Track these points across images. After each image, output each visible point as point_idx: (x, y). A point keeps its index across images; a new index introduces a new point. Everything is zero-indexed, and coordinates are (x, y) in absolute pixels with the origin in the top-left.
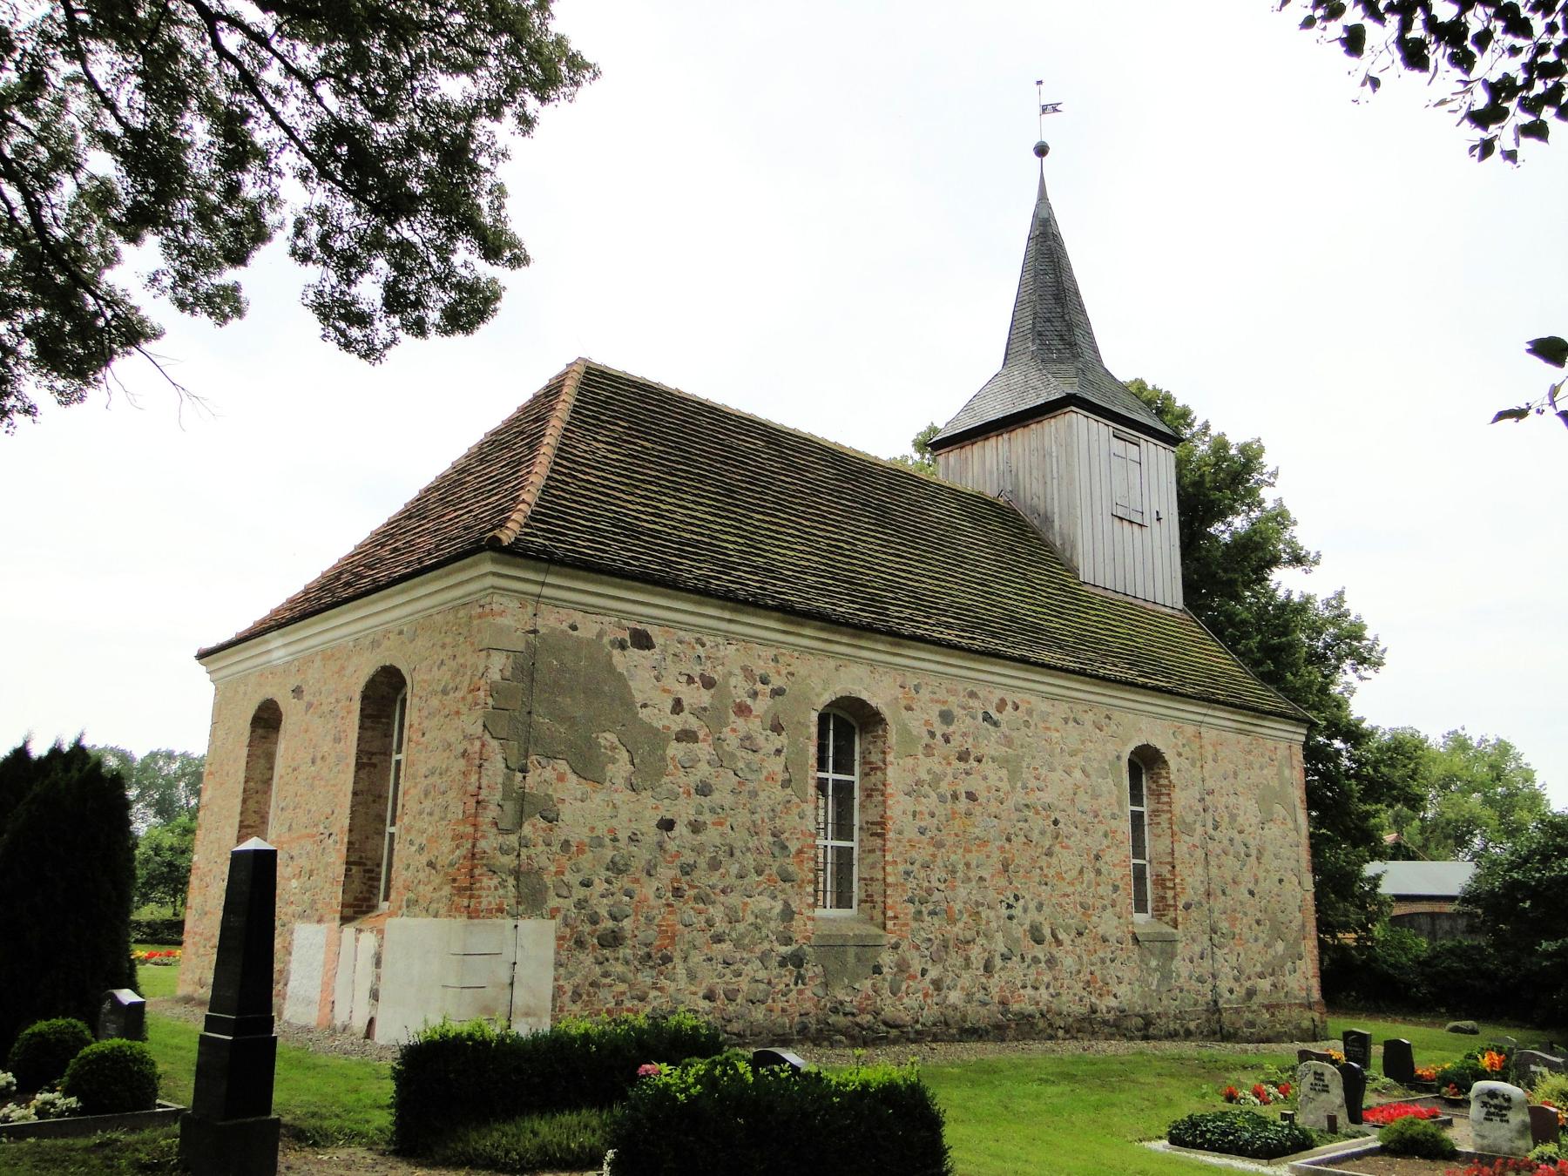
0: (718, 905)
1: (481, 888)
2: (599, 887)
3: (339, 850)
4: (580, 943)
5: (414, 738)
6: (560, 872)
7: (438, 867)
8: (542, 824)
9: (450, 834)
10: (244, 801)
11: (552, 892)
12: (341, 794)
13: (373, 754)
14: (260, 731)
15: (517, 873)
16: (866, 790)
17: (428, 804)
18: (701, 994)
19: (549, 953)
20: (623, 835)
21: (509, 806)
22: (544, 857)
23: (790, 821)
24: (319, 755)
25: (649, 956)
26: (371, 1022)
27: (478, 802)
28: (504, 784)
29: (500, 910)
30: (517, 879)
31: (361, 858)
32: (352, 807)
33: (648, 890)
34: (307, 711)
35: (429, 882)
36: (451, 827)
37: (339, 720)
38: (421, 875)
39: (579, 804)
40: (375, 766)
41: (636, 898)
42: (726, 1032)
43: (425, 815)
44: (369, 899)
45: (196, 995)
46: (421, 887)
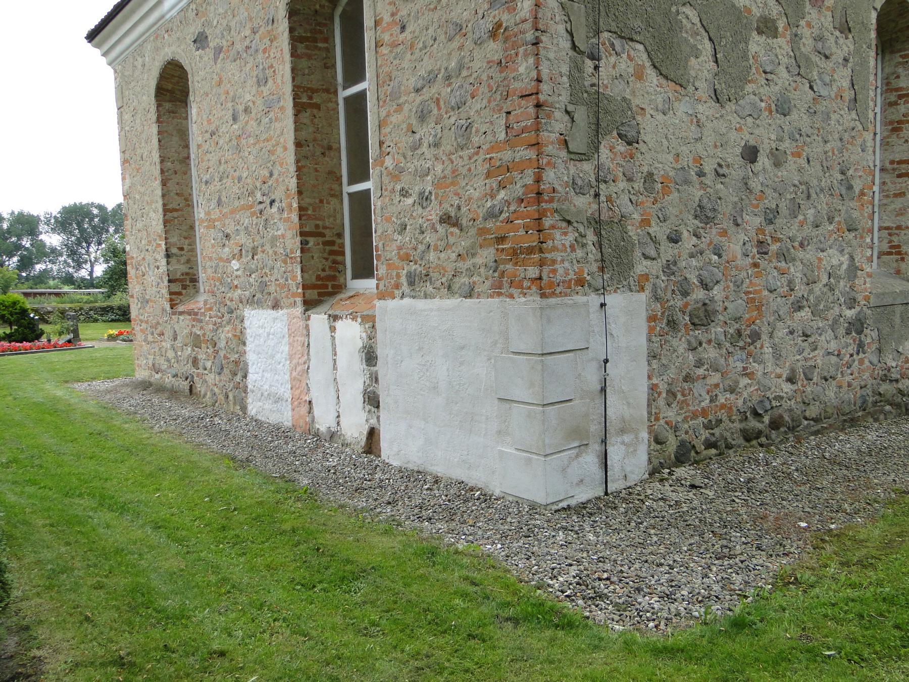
0: (798, 263)
1: (554, 249)
2: (688, 241)
3: (288, 220)
4: (672, 324)
5: (386, 37)
6: (645, 222)
7: (464, 222)
8: (621, 147)
9: (482, 168)
10: (164, 183)
11: (638, 253)
12: (280, 150)
13: (317, 91)
14: (167, 105)
15: (596, 223)
16: (891, 123)
17: (426, 132)
18: (784, 376)
19: (640, 340)
20: (709, 167)
21: (581, 114)
22: (625, 199)
23: (854, 155)
24: (241, 108)
25: (739, 333)
26: (372, 434)
27: (538, 106)
28: (570, 76)
29: (581, 282)
30: (598, 234)
31: (317, 226)
32: (297, 161)
33: (735, 247)
34: (216, 59)
35: (448, 246)
36: (482, 156)
37: (260, 55)
38: (429, 238)
39: (660, 117)
40: (317, 106)
41: (725, 257)
42: (806, 419)
43: (424, 148)
44: (334, 278)
45: (152, 380)
46: (432, 256)
